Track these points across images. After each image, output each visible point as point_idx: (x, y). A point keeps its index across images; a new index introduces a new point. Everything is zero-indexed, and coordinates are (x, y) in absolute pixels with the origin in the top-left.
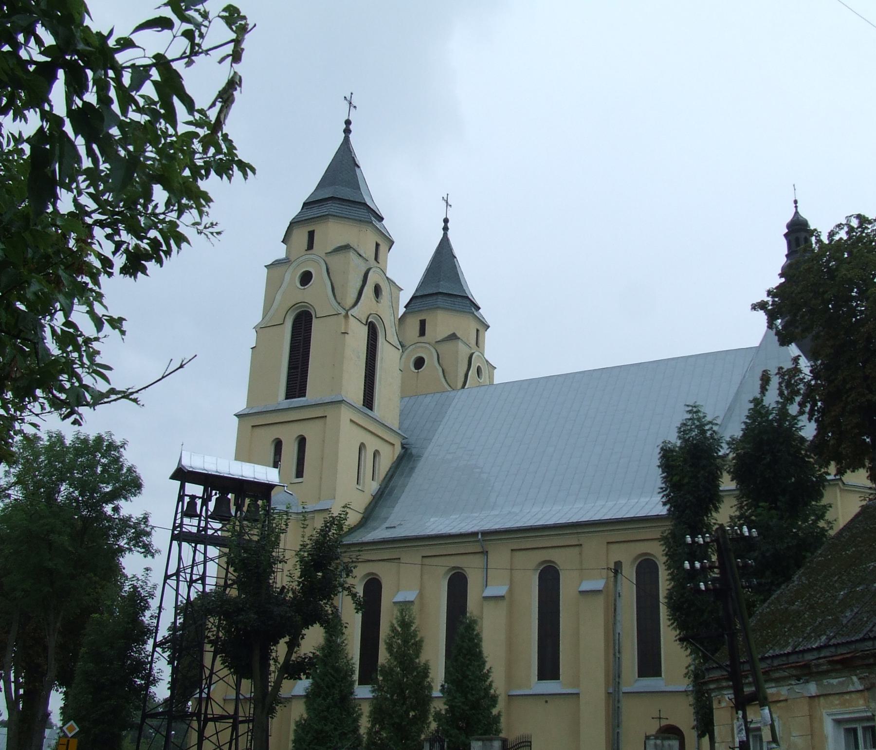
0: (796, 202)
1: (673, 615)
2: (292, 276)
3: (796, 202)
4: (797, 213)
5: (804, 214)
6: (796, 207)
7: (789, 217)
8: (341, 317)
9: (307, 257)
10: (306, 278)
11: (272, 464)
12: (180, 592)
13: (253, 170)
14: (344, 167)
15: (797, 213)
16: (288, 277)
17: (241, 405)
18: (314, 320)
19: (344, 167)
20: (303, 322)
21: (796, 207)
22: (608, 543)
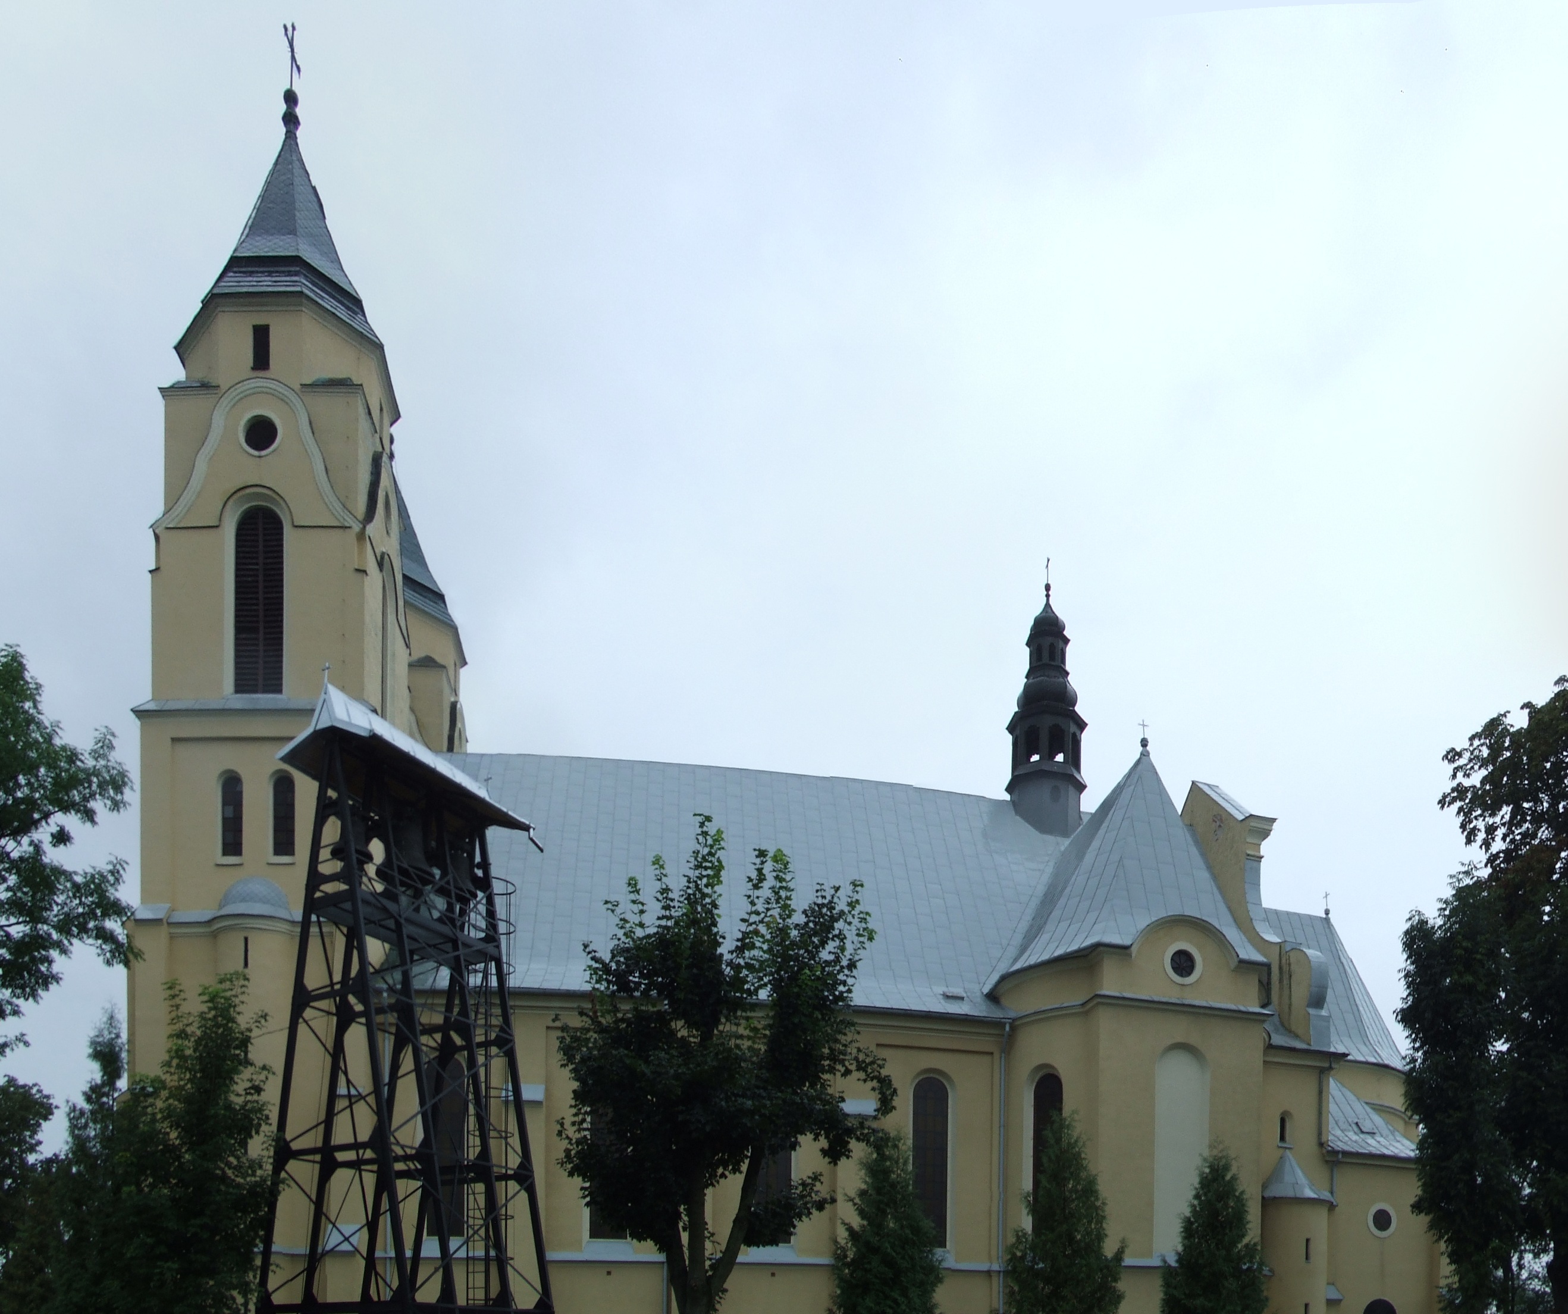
0: (1048, 587)
1: (1243, 1205)
2: (228, 423)
3: (1048, 587)
4: (1048, 605)
5: (1060, 610)
6: (1048, 596)
7: (1038, 609)
8: (351, 536)
9: (253, 384)
10: (261, 434)
11: (1255, 864)
12: (306, 1210)
13: (130, 805)
14: (288, 194)
15: (1048, 605)
16: (219, 420)
17: (143, 695)
18: (288, 532)
19: (288, 194)
20: (260, 537)
21: (1048, 596)
22: (173, 740)
